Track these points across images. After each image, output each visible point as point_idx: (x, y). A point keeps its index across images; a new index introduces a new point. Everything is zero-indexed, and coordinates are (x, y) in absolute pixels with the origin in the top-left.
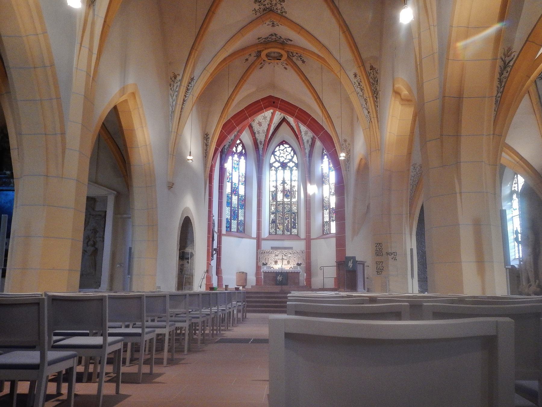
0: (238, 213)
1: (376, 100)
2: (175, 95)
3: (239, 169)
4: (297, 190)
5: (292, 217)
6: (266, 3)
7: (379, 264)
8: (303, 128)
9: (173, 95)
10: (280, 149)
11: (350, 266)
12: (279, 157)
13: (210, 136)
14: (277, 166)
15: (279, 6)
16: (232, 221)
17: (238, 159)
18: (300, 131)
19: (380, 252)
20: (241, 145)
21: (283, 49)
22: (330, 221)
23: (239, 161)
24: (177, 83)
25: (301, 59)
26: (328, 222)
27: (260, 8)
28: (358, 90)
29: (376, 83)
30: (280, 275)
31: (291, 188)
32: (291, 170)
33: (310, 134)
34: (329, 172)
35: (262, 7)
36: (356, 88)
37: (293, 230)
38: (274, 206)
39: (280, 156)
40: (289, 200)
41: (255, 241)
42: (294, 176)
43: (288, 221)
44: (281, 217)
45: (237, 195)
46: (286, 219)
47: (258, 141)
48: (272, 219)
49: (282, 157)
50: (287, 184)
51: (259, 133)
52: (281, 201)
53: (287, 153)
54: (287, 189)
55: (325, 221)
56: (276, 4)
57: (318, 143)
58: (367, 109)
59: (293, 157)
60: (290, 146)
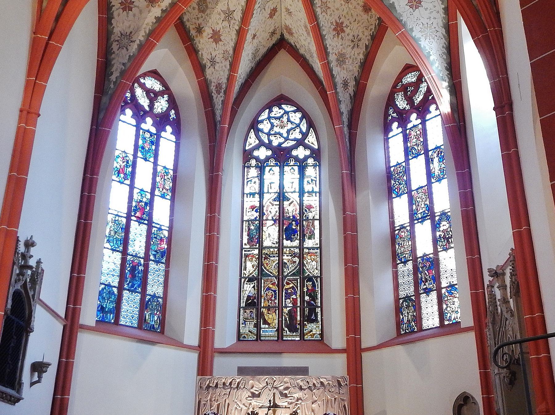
0: (146, 272)
5: (305, 290)
12: (269, 134)
14: (262, 157)
16: (126, 294)
18: (323, 51)
22: (417, 294)
23: (159, 137)
26: (413, 298)
31: (301, 213)
32: (302, 166)
34: (407, 160)
37: (310, 326)
39: (272, 132)
40: (296, 243)
41: (194, 357)
43: (294, 302)
44: (275, 291)
45: (146, 222)
46: (288, 296)
47: (213, 88)
48: (246, 296)
50: (290, 201)
51: (213, 62)
52: (274, 246)
54: (291, 214)
55: (402, 294)
59: (305, 135)
60: (299, 109)
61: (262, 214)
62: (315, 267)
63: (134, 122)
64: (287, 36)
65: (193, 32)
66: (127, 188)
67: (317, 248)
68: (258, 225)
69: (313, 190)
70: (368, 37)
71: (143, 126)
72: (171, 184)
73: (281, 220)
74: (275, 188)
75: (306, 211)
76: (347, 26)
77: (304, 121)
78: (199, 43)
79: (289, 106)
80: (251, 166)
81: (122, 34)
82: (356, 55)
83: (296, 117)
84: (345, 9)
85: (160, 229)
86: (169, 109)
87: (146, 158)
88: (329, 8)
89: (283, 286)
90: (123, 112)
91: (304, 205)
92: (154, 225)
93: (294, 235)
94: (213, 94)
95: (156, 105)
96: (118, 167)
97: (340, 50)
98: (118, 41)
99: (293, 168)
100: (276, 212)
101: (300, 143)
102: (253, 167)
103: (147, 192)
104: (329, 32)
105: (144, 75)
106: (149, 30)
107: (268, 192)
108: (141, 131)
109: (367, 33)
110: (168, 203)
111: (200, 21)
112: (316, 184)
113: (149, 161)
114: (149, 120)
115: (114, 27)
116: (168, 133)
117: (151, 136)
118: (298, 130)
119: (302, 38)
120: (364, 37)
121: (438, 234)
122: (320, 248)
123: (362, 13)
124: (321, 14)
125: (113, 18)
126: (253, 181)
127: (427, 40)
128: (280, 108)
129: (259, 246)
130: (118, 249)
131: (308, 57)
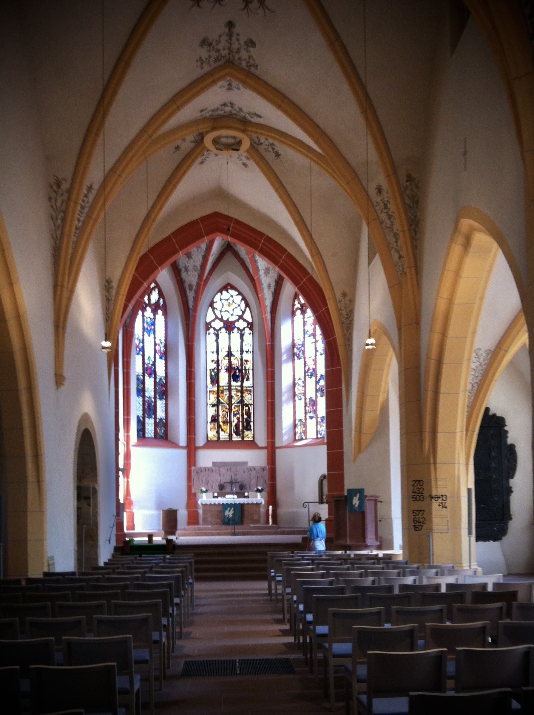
1: (414, 235)
2: (60, 217)
3: (154, 334)
4: (251, 368)
6: (220, 46)
7: (417, 513)
8: (262, 263)
9: (57, 218)
11: (355, 504)
13: (115, 284)
15: (244, 54)
17: (152, 316)
18: (257, 269)
19: (420, 495)
20: (157, 290)
21: (244, 131)
23: (155, 318)
24: (62, 195)
25: (273, 149)
27: (210, 57)
28: (383, 216)
29: (415, 206)
30: (229, 509)
31: (242, 365)
33: (275, 272)
35: (214, 54)
36: (379, 212)
37: (246, 433)
42: (247, 344)
43: (238, 419)
51: (187, 269)
53: (234, 306)
56: (239, 50)
57: (289, 288)
58: (398, 251)
59: (244, 312)
60: (240, 293)
61: (218, 365)
62: (250, 398)
67: (251, 387)
77: (243, 302)
89: (232, 409)
91: (244, 360)
93: (238, 379)
100: (227, 364)
114: (148, 309)
116: (160, 317)
121: (318, 387)
122: (253, 387)
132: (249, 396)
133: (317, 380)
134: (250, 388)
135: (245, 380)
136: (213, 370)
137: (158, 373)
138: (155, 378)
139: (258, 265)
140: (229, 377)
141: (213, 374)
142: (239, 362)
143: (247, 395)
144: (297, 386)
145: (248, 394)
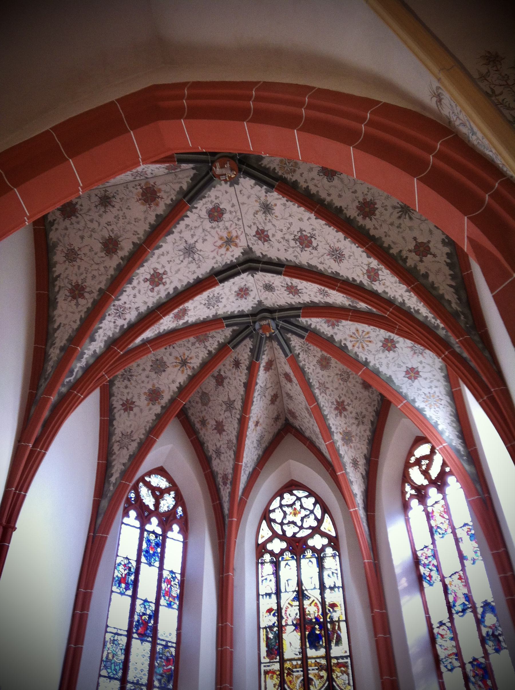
4: (343, 618)
10: (284, 502)
12: (282, 524)
14: (277, 551)
18: (327, 432)
20: (173, 494)
23: (164, 536)
31: (324, 614)
38: (275, 676)
40: (322, 652)
42: (331, 575)
47: (220, 480)
49: (289, 523)
50: (311, 600)
59: (320, 522)
60: (311, 494)
61: (280, 618)
62: (347, 682)
63: (137, 524)
64: (291, 420)
65: (198, 426)
66: (129, 600)
67: (346, 657)
68: (277, 632)
69: (335, 585)
70: (372, 414)
71: (148, 527)
72: (178, 591)
73: (302, 625)
74: (293, 586)
75: (329, 610)
76: (349, 405)
77: (318, 506)
78: (204, 436)
79: (301, 492)
80: (265, 562)
81: (123, 434)
82: (363, 432)
83: (309, 502)
84: (344, 388)
85: (166, 647)
86: (175, 507)
87: (150, 563)
88: (328, 388)
90: (126, 514)
91: (327, 603)
92: (159, 641)
93: (319, 643)
94: (220, 486)
95: (162, 503)
96: (120, 576)
97: (344, 429)
98: (119, 441)
99: (310, 561)
100: (297, 614)
101: (316, 530)
102: (267, 563)
103: (151, 602)
104: (330, 412)
105: (149, 474)
106: (150, 428)
107: (286, 591)
108: (146, 533)
109: (370, 409)
110: (176, 613)
111: (204, 413)
112: (337, 577)
113: (153, 566)
114: (154, 520)
115: (115, 428)
117: (156, 537)
118: (312, 517)
119: (306, 420)
120: (367, 414)
122: (350, 656)
123: (363, 391)
124: (320, 394)
125: (115, 419)
126: (268, 580)
127: (433, 410)
128: (292, 494)
129: (280, 659)
130: (117, 676)
131: (314, 438)
132: (345, 677)
133: (479, 616)
134: (345, 660)
135: (333, 645)
136: (271, 628)
137: (161, 634)
138: (154, 644)
139: (329, 424)
140: (301, 639)
141: (271, 636)
142: (318, 609)
143: (339, 674)
144: (439, 640)
145: (343, 672)
